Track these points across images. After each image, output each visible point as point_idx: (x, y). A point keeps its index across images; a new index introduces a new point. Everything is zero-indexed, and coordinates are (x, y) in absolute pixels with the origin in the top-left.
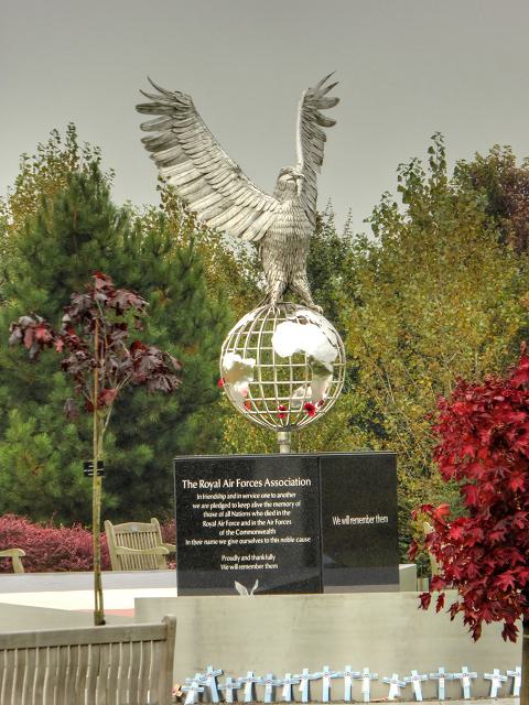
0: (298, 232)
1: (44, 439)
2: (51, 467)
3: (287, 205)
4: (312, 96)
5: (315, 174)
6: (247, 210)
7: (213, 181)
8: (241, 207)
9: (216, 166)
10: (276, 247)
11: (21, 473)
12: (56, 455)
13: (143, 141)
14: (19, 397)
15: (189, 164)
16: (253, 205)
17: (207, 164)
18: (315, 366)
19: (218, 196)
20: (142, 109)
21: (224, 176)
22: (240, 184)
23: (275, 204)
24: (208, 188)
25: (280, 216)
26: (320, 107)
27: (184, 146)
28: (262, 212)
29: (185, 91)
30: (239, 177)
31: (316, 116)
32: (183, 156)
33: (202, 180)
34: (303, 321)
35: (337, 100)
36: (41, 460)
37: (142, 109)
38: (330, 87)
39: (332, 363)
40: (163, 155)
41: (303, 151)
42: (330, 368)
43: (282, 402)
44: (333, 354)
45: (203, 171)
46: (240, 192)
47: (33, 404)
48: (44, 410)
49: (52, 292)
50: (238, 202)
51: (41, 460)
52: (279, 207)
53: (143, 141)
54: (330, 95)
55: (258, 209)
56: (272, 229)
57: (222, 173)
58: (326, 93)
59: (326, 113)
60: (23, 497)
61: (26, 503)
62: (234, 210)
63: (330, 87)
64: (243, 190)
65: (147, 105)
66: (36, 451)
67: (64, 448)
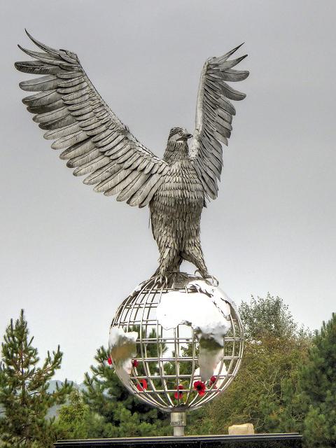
0: (187, 194)
1: (322, 416)
2: (325, 427)
3: (176, 167)
4: (217, 65)
5: (221, 146)
6: (136, 174)
7: (100, 144)
8: (128, 171)
9: (103, 128)
10: (165, 212)
11: (314, 430)
12: (328, 423)
13: (24, 101)
14: (315, 399)
15: (75, 126)
16: (142, 167)
17: (93, 126)
18: (203, 339)
19: (106, 160)
20: (21, 67)
21: (111, 138)
22: (128, 147)
23: (164, 166)
24: (95, 152)
25: (168, 178)
26: (226, 78)
27: (70, 108)
28: (150, 175)
29: (69, 49)
30: (127, 138)
31: (222, 87)
32: (69, 118)
33: (89, 144)
34: (194, 290)
35: (246, 74)
36: (321, 424)
37: (21, 67)
38: (239, 60)
39: (224, 336)
40: (47, 117)
41: (204, 119)
42: (221, 342)
43: (183, 379)
44: (223, 327)
45: (90, 133)
46: (128, 155)
47: (319, 403)
48: (323, 405)
49: (327, 358)
50: (126, 165)
51: (321, 424)
52: (167, 168)
53: (24, 101)
54: (239, 68)
55: (147, 171)
56: (161, 193)
57: (110, 135)
58: (228, 57)
59: (235, 86)
60: (315, 439)
61: (316, 441)
62: (122, 174)
63: (239, 60)
64: (131, 152)
65: (27, 64)
66: (319, 421)
67: (331, 420)
